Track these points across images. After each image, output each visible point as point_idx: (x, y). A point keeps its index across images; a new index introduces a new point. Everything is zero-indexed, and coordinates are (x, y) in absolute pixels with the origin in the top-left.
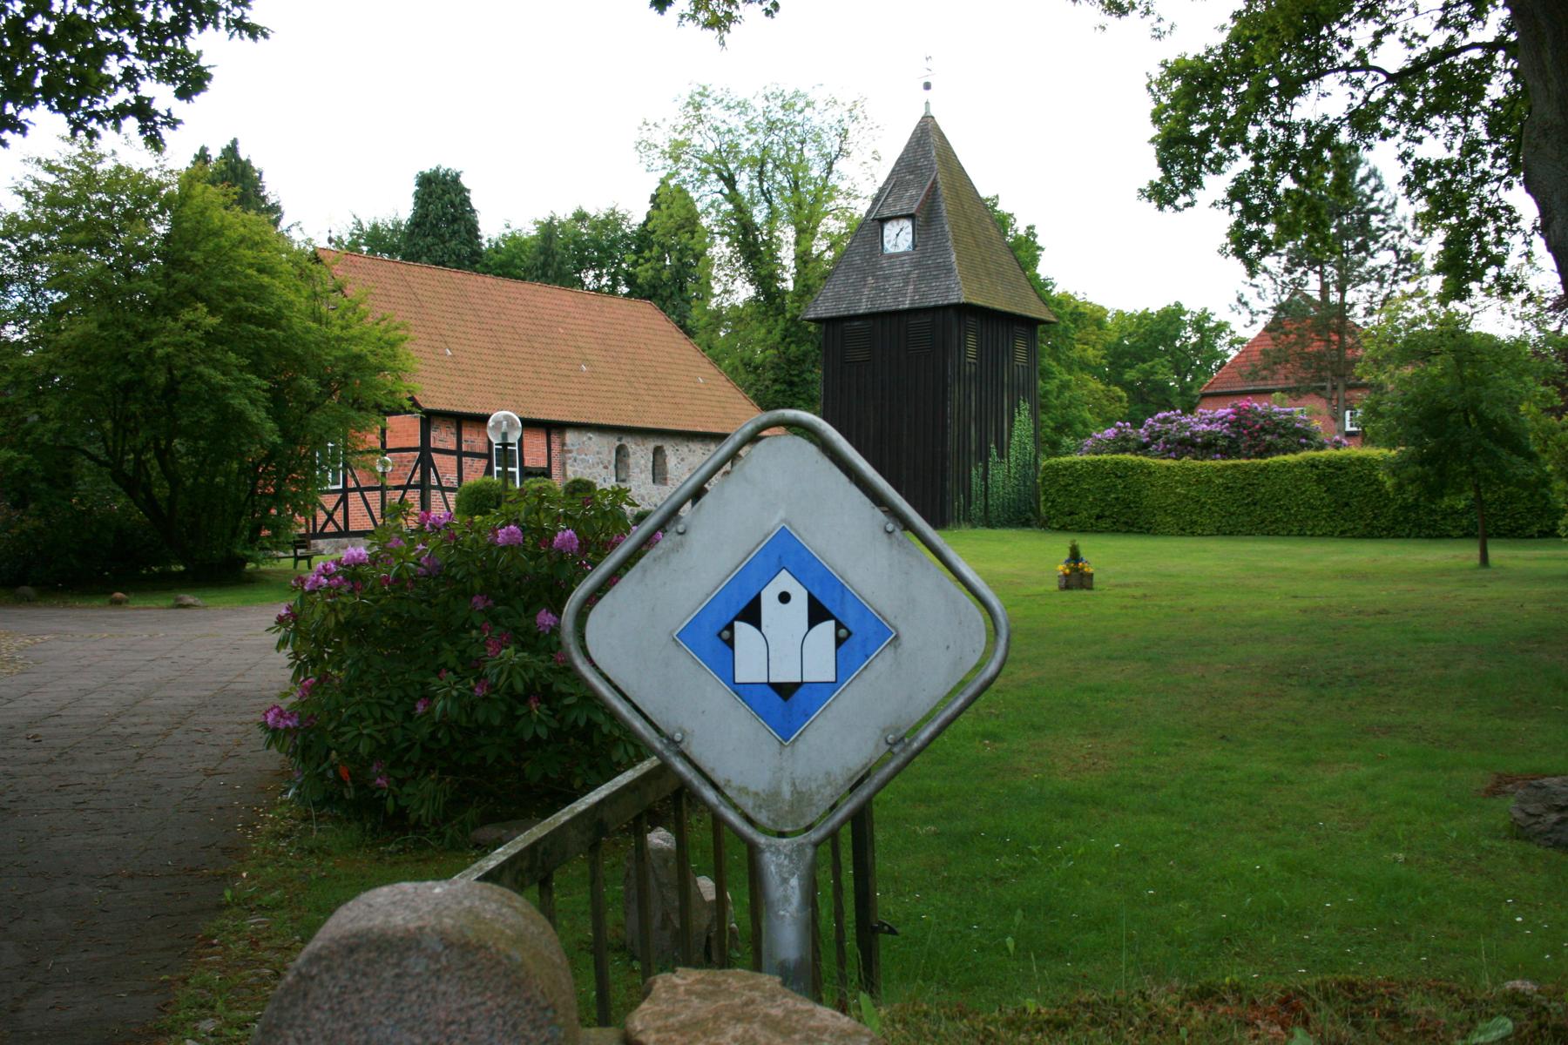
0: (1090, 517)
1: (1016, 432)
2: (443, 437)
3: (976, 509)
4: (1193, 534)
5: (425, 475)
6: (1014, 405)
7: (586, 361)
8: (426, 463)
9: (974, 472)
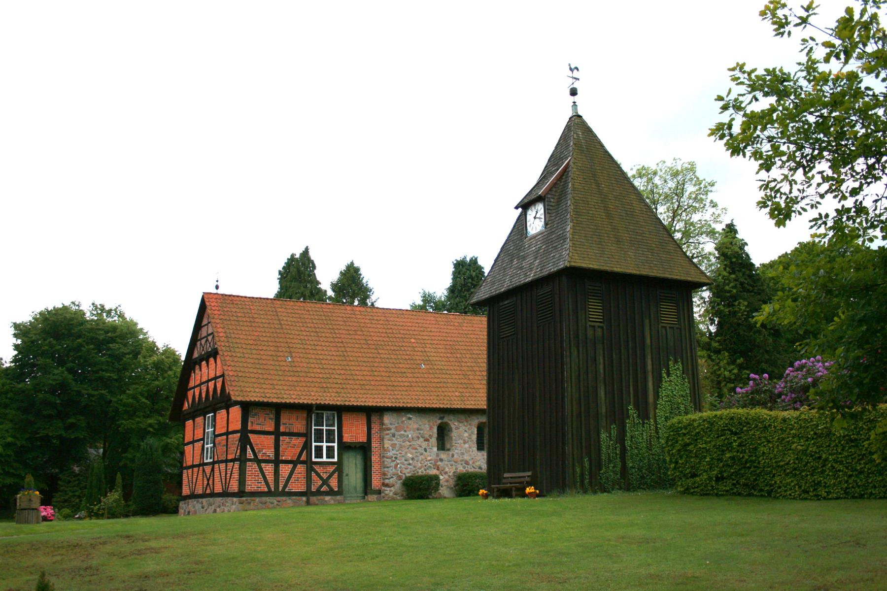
0: (710, 478)
1: (663, 393)
2: (262, 422)
3: (610, 471)
4: (818, 497)
6: (660, 366)
7: (427, 362)
8: (245, 442)
9: (603, 436)
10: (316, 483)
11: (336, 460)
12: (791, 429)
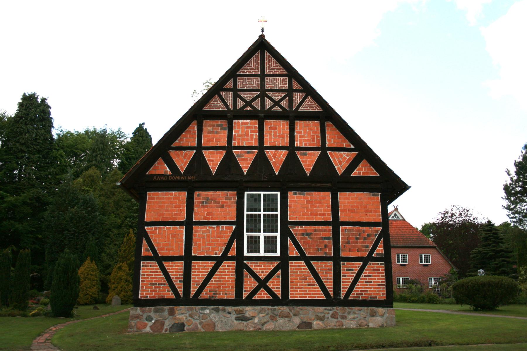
10: (250, 284)
11: (278, 254)
12: (309, 242)
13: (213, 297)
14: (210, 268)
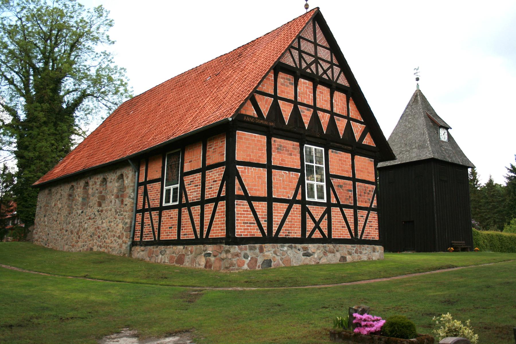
5: (230, 188)
11: (325, 200)
13: (287, 235)
14: (285, 210)
